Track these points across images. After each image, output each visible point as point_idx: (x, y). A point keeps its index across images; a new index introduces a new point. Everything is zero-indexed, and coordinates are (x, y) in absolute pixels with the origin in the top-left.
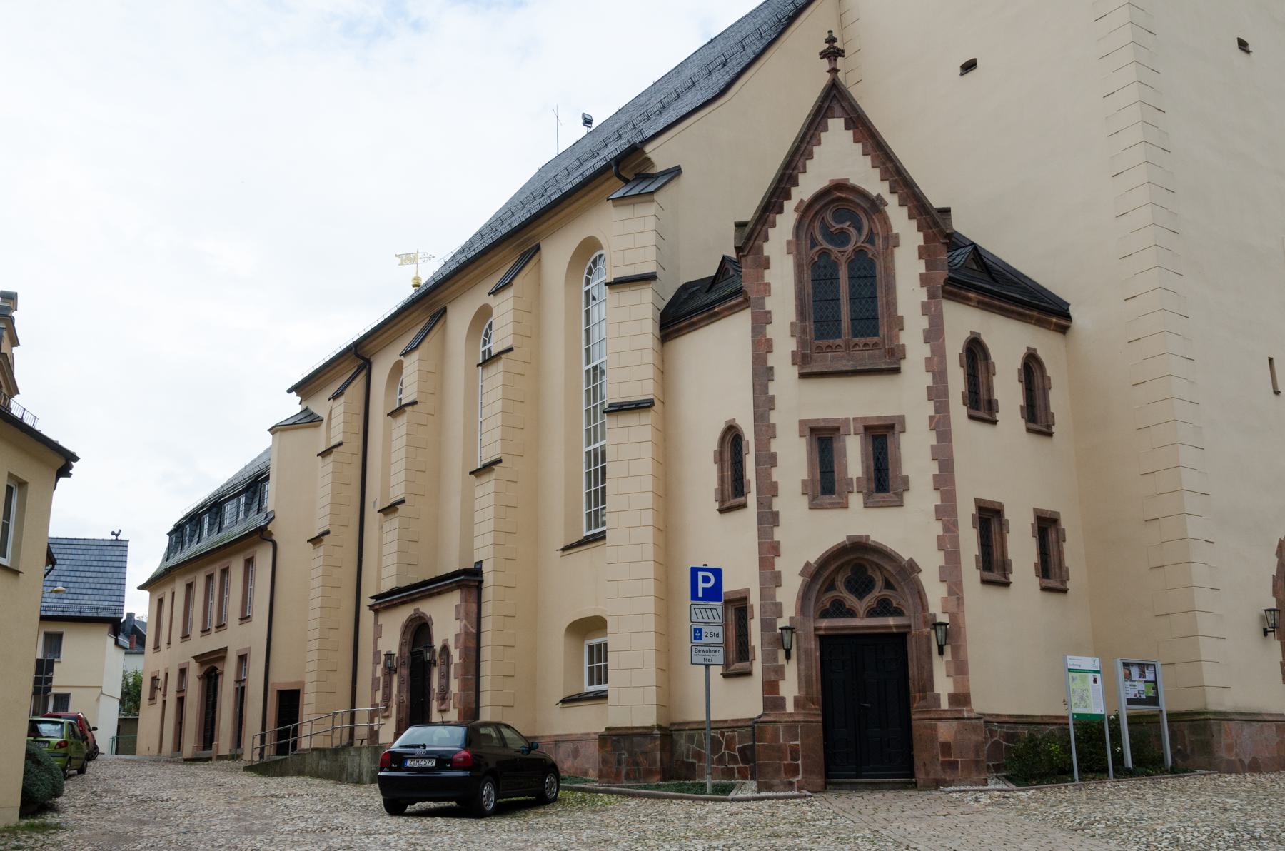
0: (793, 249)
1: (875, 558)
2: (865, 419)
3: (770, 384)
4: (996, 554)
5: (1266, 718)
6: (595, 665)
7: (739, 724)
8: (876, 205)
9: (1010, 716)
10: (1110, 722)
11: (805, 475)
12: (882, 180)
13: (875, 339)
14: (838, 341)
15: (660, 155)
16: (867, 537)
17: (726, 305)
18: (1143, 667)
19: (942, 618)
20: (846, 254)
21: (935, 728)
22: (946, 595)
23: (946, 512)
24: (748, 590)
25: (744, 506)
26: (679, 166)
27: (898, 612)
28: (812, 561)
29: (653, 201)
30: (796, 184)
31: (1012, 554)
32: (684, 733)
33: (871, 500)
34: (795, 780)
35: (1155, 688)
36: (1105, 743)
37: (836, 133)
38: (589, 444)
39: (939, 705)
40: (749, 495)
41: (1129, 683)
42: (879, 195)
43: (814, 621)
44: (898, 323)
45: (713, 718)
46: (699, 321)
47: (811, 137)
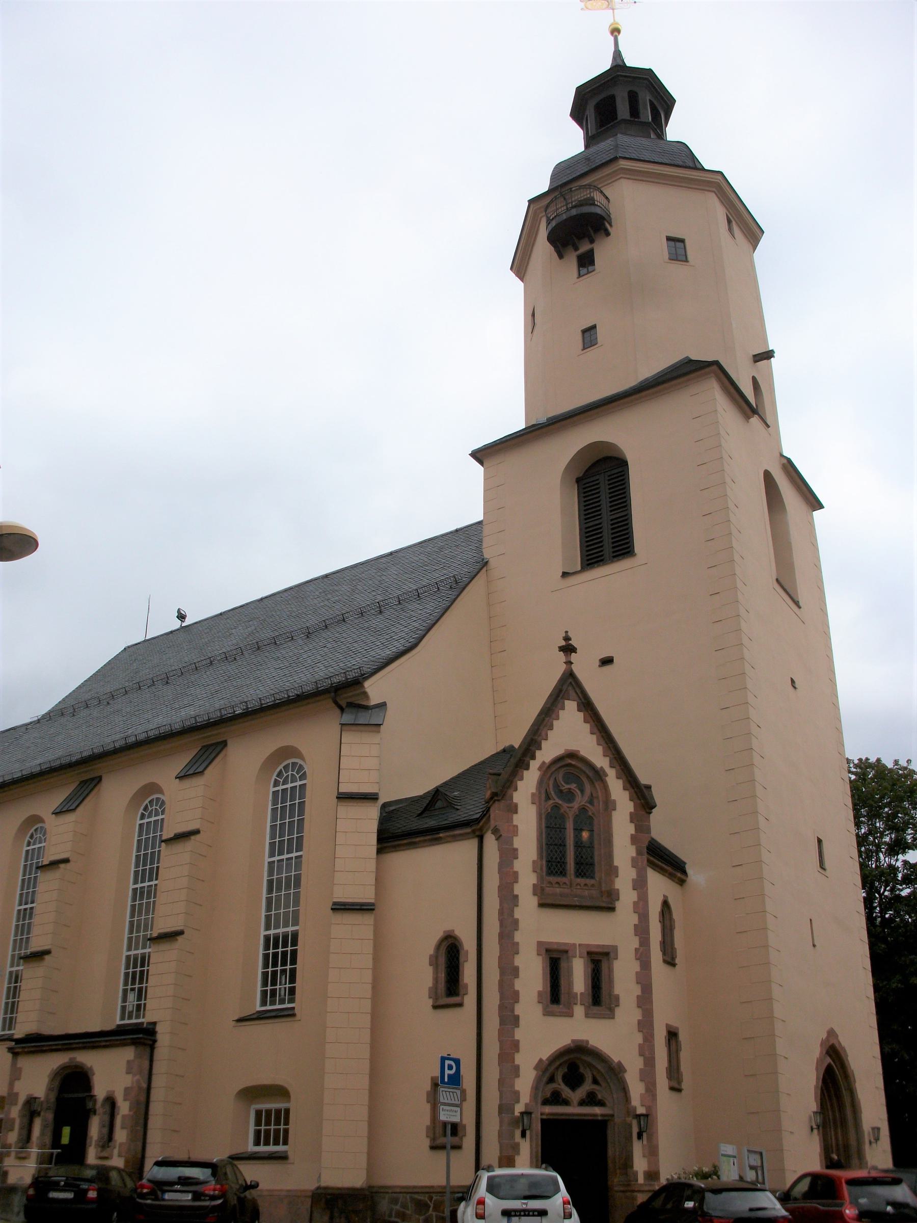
1: (589, 1059)
2: (588, 945)
3: (516, 909)
8: (598, 775)
14: (564, 880)
19: (641, 1110)
20: (573, 809)
23: (646, 1025)
26: (385, 702)
27: (601, 1104)
28: (544, 1059)
30: (540, 748)
32: (387, 1196)
37: (570, 713)
38: (129, 949)
40: (466, 997)
42: (602, 767)
44: (613, 871)
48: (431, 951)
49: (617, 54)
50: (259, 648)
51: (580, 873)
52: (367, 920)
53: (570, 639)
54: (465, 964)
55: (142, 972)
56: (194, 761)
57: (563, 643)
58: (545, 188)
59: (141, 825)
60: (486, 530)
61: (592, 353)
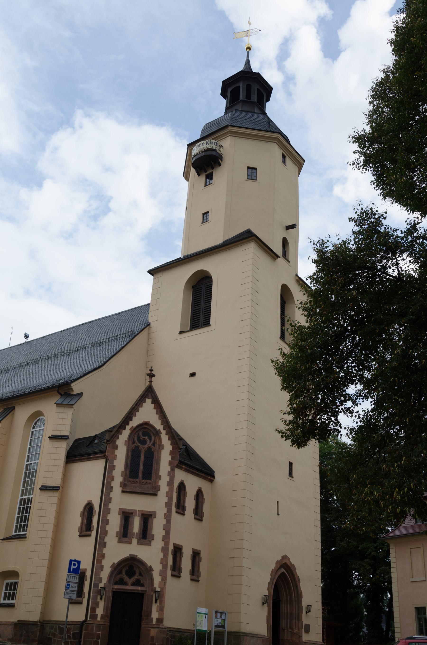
0: (127, 444)
5: (259, 636)
6: (8, 591)
7: (74, 623)
8: (158, 433)
9: (174, 628)
10: (208, 633)
11: (118, 529)
12: (161, 424)
13: (150, 481)
14: (137, 480)
15: (76, 388)
16: (137, 556)
17: (95, 456)
18: (221, 613)
19: (158, 589)
21: (150, 631)
22: (160, 581)
23: (165, 550)
24: (86, 569)
25: (90, 535)
27: (142, 585)
28: (116, 562)
29: (72, 408)
30: (132, 420)
32: (49, 625)
33: (140, 542)
35: (224, 622)
36: (205, 641)
37: (148, 404)
38: (22, 496)
39: (152, 622)
40: (92, 532)
41: (216, 619)
42: (159, 430)
43: (112, 586)
44: (159, 477)
45: (68, 620)
46: (83, 459)
47: (139, 404)
50: (48, 359)
51: (144, 478)
53: (153, 371)
54: (94, 516)
56: (3, 412)
57: (149, 372)
60: (151, 308)
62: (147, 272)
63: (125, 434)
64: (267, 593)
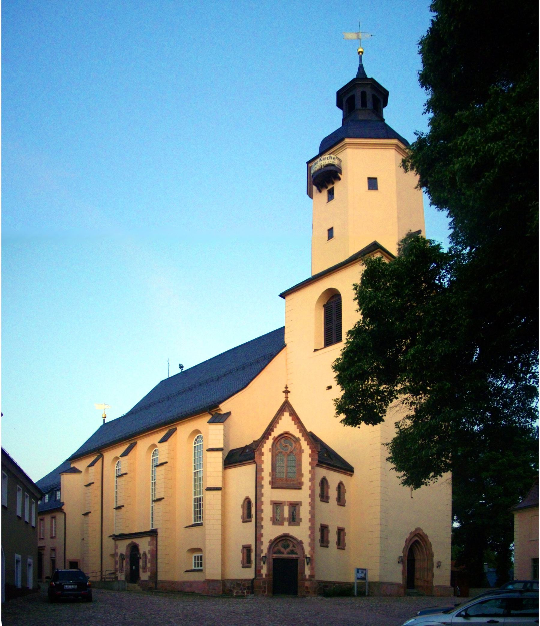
0: (271, 450)
4: (325, 539)
8: (297, 440)
19: (309, 556)
21: (304, 583)
23: (312, 529)
27: (296, 554)
30: (273, 431)
31: (330, 539)
34: (265, 594)
38: (195, 495)
48: (242, 503)
49: (361, 68)
52: (219, 492)
55: (200, 504)
57: (285, 389)
58: (318, 153)
59: (195, 447)
61: (332, 241)
62: (279, 296)
63: (269, 443)
64: (402, 555)
